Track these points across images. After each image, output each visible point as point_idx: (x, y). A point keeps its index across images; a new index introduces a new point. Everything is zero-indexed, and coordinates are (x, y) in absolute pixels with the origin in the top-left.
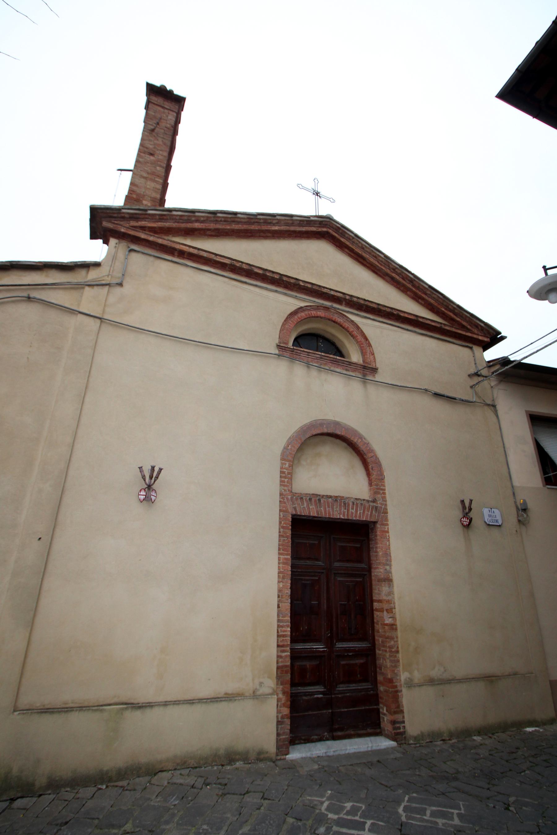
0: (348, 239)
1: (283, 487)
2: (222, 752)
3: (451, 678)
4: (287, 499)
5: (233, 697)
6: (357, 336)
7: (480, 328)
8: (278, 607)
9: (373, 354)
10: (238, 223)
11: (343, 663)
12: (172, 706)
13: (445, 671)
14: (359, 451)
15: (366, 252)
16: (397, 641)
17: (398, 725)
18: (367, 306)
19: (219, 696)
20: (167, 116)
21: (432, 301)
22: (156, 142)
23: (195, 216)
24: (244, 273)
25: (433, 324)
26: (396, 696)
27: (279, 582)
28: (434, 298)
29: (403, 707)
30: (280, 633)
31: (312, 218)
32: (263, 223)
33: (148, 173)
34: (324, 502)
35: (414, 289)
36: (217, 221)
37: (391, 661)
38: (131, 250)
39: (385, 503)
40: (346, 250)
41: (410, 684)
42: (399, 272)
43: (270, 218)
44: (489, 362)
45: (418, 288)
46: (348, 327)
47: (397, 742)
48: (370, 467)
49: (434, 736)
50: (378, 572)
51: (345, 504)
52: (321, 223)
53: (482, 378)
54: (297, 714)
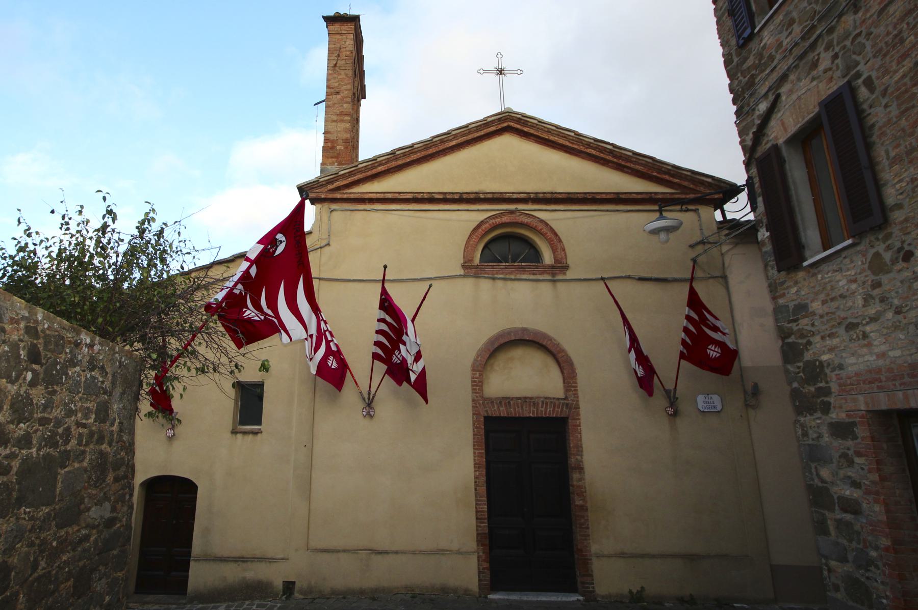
0: (532, 126)
8: (476, 489)
9: (564, 250)
15: (553, 134)
26: (586, 563)
31: (489, 120)
50: (572, 460)
51: (534, 404)
52: (499, 119)
53: (709, 246)
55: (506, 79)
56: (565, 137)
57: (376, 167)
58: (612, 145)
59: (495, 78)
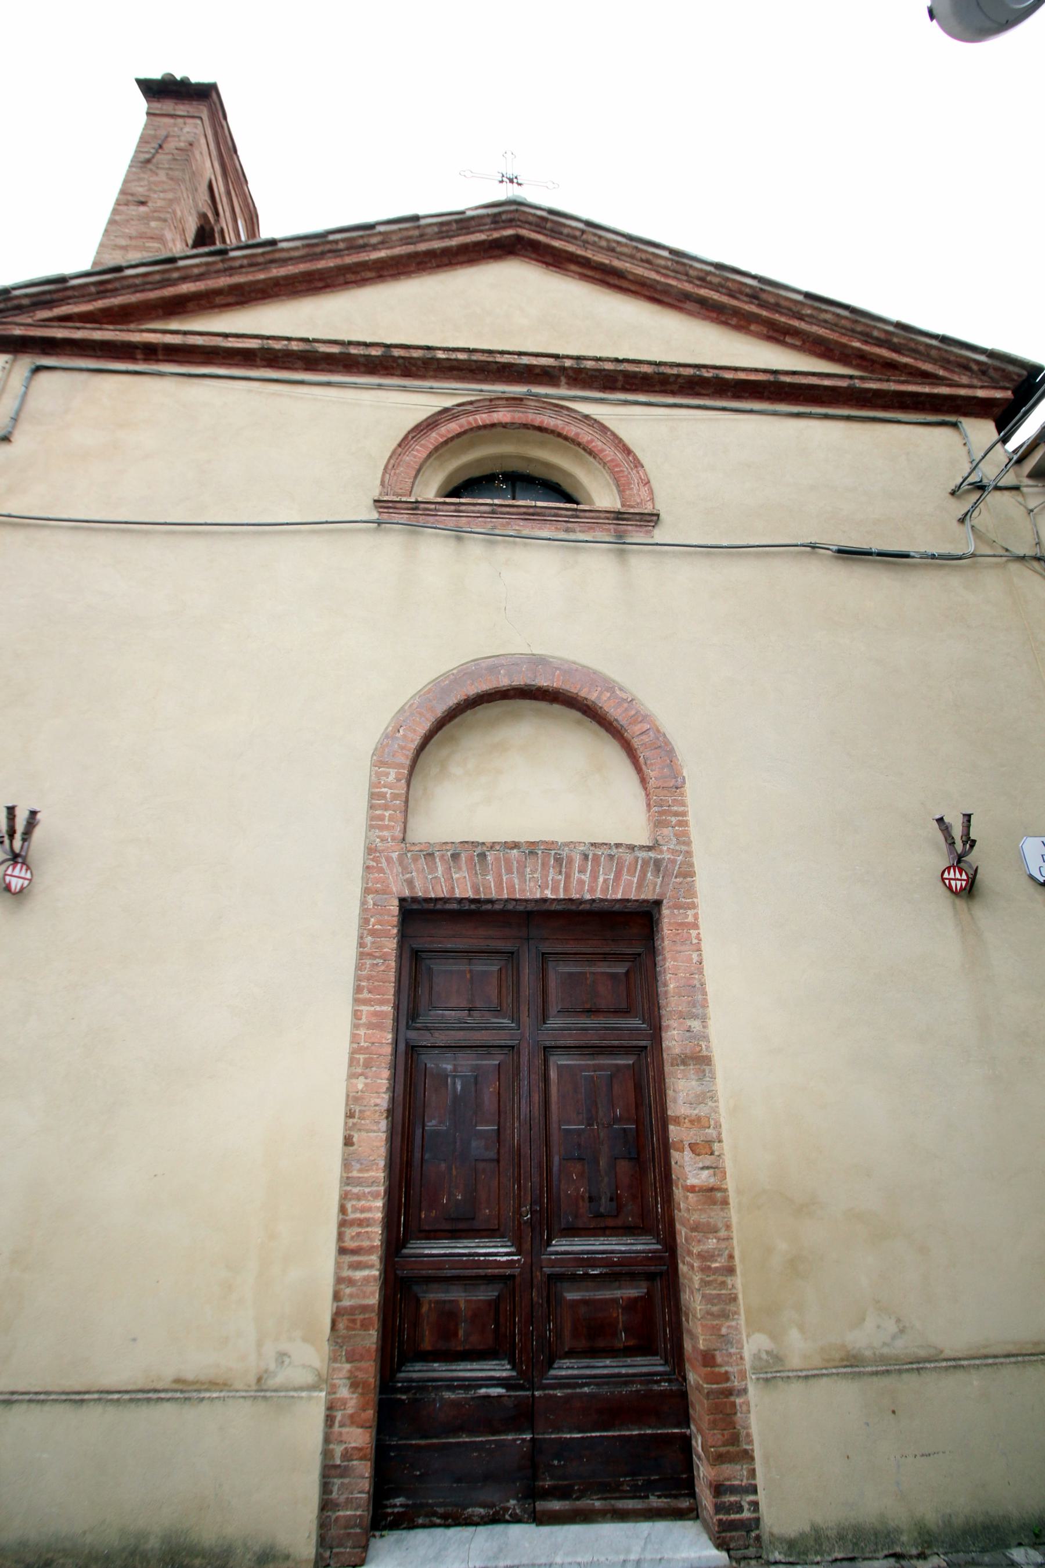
0: (571, 238)
1: (377, 832)
2: (153, 1543)
3: (922, 1353)
4: (389, 860)
5: (199, 1391)
6: (602, 450)
7: (975, 367)
8: (348, 1142)
10: (284, 262)
11: (571, 1296)
12: (24, 1407)
13: (902, 1331)
14: (611, 724)
15: (620, 256)
16: (729, 1238)
17: (733, 1499)
18: (626, 374)
19: (159, 1386)
20: (181, 129)
21: (822, 332)
22: (154, 179)
23: (178, 269)
24: (300, 364)
25: (827, 382)
26: (726, 1405)
27: (352, 1076)
28: (826, 321)
29: (751, 1442)
30: (352, 1216)
31: (470, 213)
32: (348, 249)
33: (131, 238)
34: (497, 859)
35: (764, 313)
36: (232, 268)
37: (708, 1299)
38: (38, 369)
39: (684, 848)
40: (573, 267)
41: (774, 1372)
42: (716, 280)
43: (361, 233)
44: (1013, 452)
45: (776, 307)
46: (577, 434)
47: (728, 1550)
48: (641, 760)
49: (857, 1542)
51: (558, 860)
54: (423, 1442)
57: (174, 283)
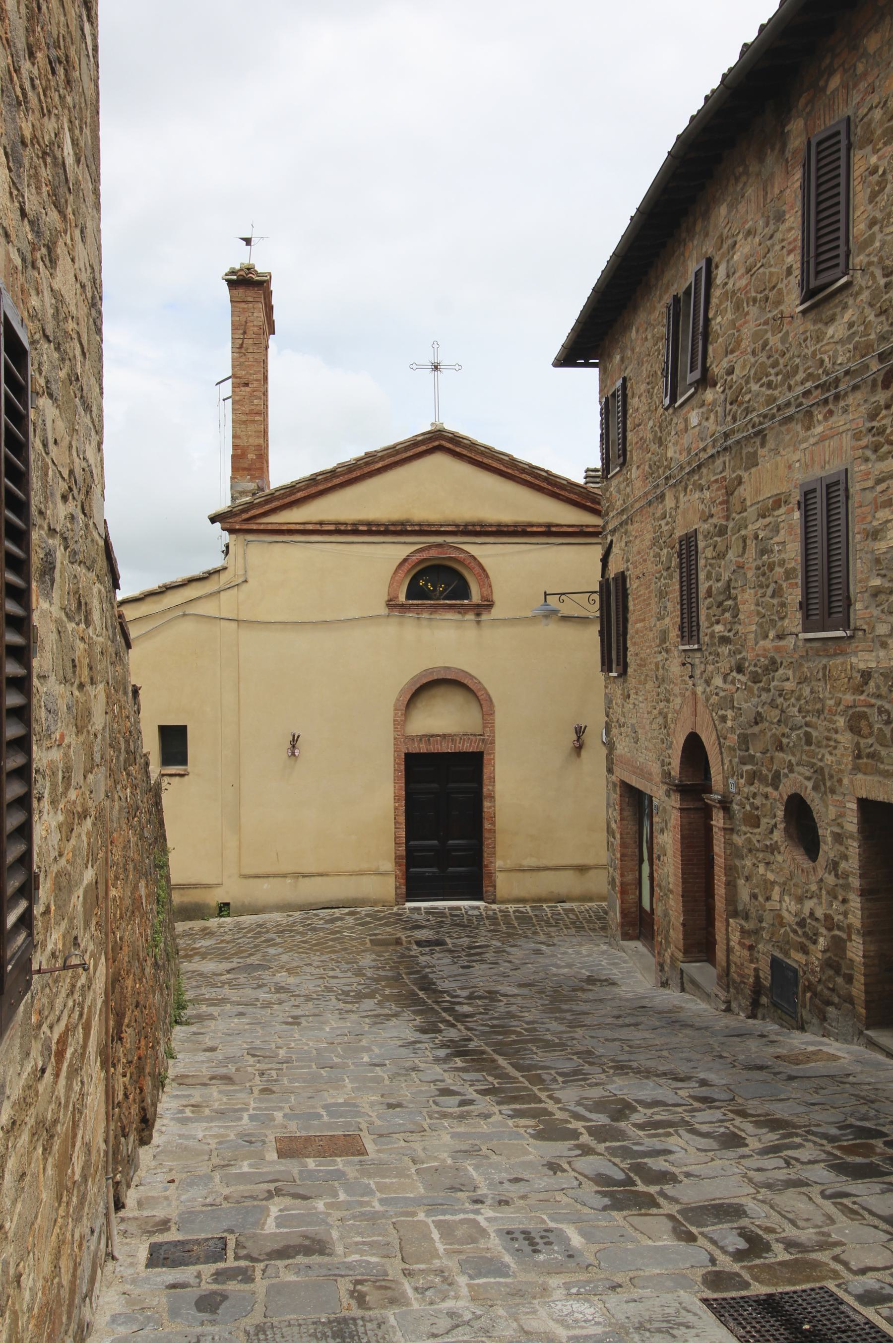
0: (465, 447)
15: (487, 457)
26: (491, 875)
52: (430, 438)
55: (443, 375)
56: (500, 461)
57: (294, 494)
58: (547, 472)
59: (428, 374)
